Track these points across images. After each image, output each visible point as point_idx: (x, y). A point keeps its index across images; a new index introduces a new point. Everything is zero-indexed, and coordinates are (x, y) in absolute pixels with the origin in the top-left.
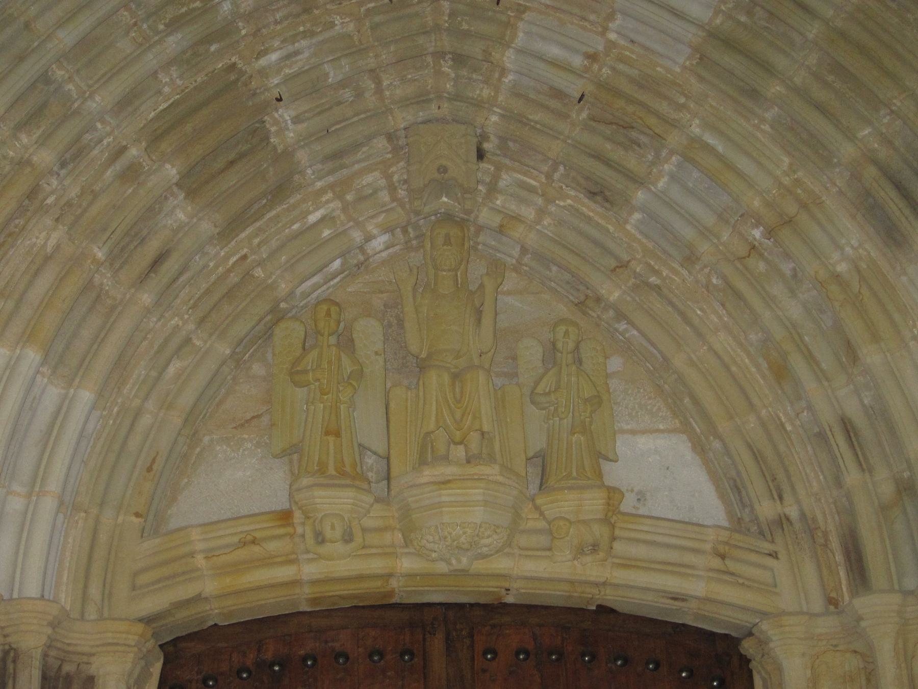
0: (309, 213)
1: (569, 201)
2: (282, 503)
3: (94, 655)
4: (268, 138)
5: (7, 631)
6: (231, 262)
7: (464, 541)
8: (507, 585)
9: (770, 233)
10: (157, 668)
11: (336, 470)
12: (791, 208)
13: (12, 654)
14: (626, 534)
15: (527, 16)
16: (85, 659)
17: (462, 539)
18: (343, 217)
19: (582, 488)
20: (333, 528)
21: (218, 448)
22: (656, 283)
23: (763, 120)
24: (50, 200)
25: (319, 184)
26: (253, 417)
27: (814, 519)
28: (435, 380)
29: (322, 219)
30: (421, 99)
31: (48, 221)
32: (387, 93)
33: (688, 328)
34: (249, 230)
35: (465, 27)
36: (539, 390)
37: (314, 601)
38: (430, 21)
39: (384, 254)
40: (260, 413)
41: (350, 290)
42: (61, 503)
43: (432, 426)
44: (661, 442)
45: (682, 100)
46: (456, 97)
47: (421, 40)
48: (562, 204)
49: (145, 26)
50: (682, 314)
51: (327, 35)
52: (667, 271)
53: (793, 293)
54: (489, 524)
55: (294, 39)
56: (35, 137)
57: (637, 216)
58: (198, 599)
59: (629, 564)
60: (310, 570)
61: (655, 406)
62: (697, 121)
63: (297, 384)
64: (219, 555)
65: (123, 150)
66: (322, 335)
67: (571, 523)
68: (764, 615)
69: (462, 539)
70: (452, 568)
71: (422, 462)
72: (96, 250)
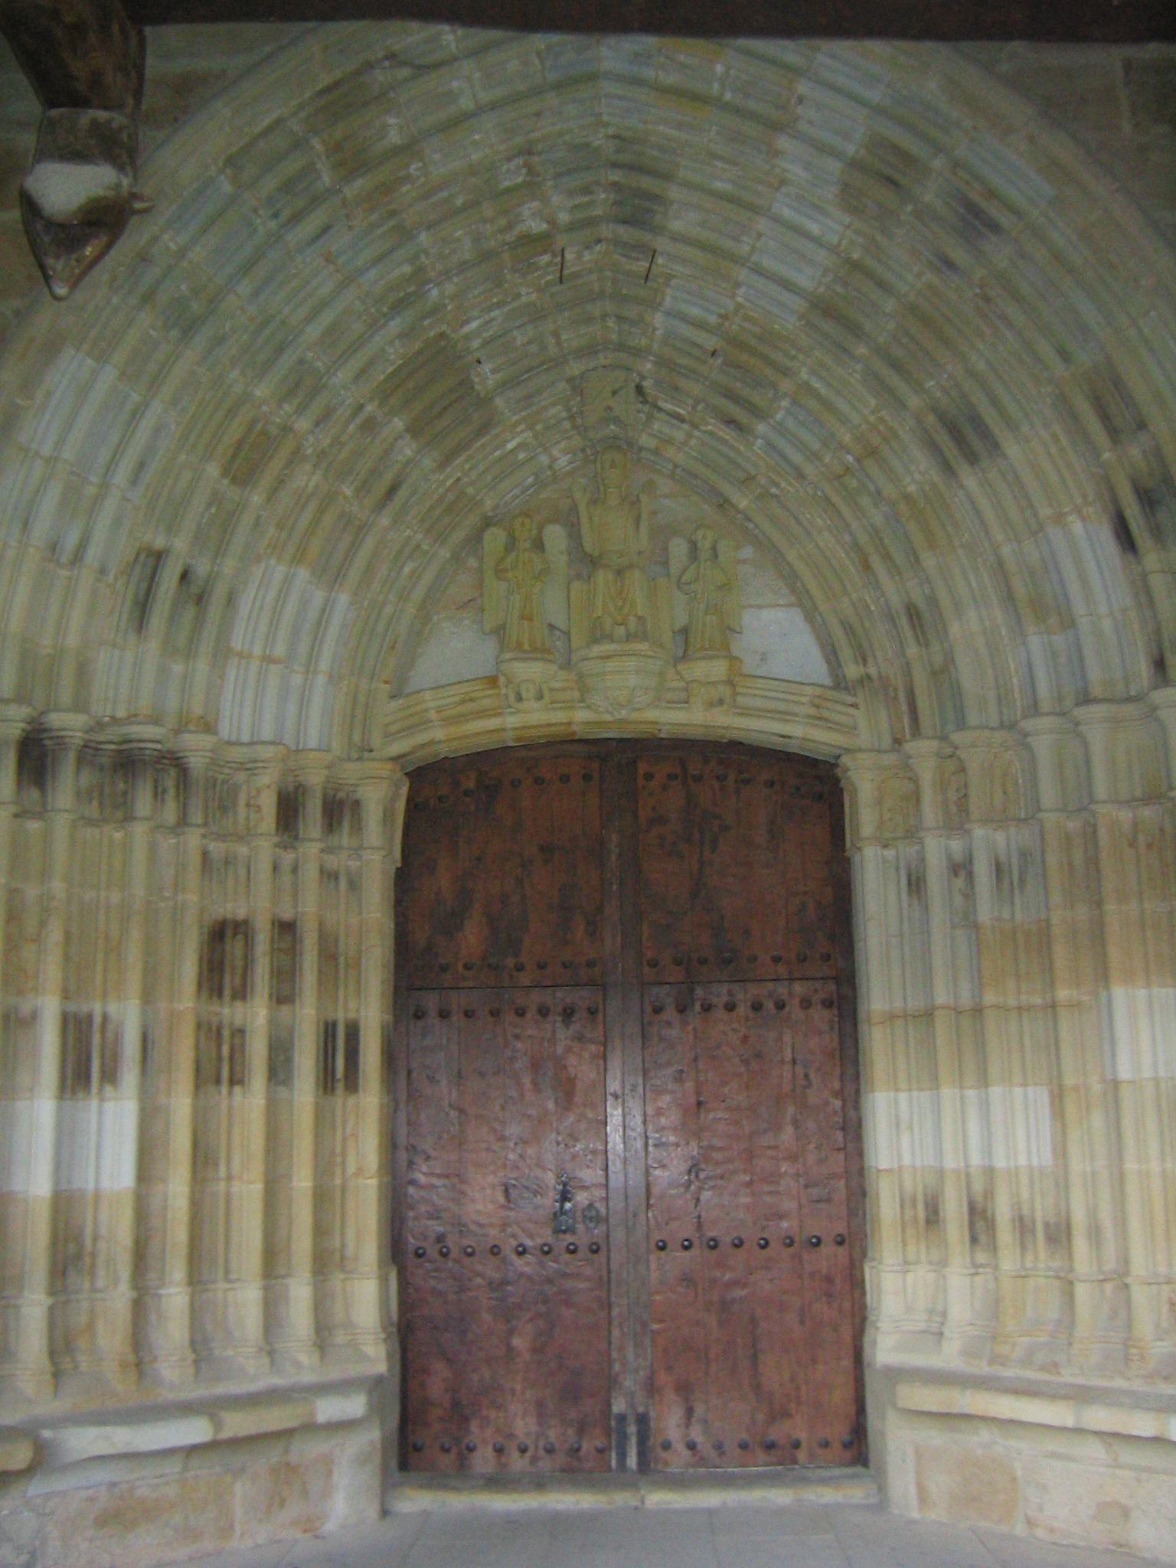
0: (508, 442)
1: (710, 427)
2: (487, 670)
3: (357, 785)
4: (472, 388)
5: (296, 773)
6: (448, 484)
8: (659, 728)
9: (858, 460)
10: (404, 791)
12: (876, 440)
13: (301, 790)
14: (745, 691)
15: (673, 282)
16: (352, 789)
18: (534, 443)
19: (712, 658)
23: (855, 371)
24: (309, 451)
25: (515, 418)
27: (888, 678)
28: (603, 578)
29: (519, 447)
30: (590, 350)
31: (308, 467)
32: (565, 345)
34: (462, 458)
35: (625, 291)
36: (684, 579)
37: (519, 739)
38: (596, 287)
39: (567, 468)
42: (331, 676)
43: (600, 613)
44: (780, 614)
45: (794, 352)
46: (621, 347)
47: (589, 307)
49: (373, 310)
50: (796, 518)
51: (516, 304)
53: (876, 506)
55: (490, 309)
56: (295, 404)
57: (760, 441)
58: (432, 742)
59: (746, 711)
60: (511, 721)
62: (805, 369)
63: (500, 579)
65: (361, 407)
68: (847, 750)
71: (595, 641)
72: (346, 490)
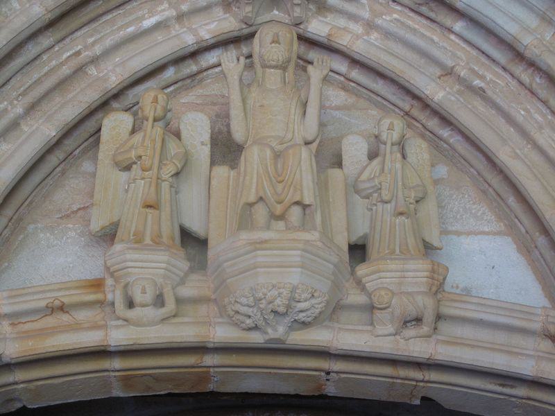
0: (143, 18)
1: (395, 16)
7: (280, 303)
11: (152, 240)
17: (278, 301)
20: (144, 292)
21: (42, 235)
22: (480, 86)
26: (79, 209)
33: (512, 129)
40: (86, 205)
41: (183, 101)
48: (388, 18)
52: (491, 76)
54: (307, 286)
61: (479, 210)
64: (25, 323)
66: (147, 120)
67: (393, 294)
69: (278, 301)
70: (267, 337)
